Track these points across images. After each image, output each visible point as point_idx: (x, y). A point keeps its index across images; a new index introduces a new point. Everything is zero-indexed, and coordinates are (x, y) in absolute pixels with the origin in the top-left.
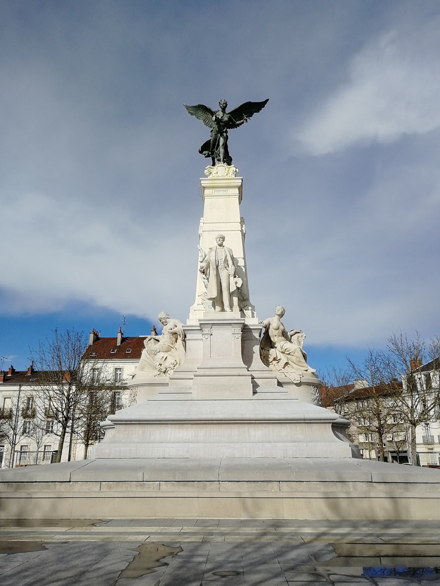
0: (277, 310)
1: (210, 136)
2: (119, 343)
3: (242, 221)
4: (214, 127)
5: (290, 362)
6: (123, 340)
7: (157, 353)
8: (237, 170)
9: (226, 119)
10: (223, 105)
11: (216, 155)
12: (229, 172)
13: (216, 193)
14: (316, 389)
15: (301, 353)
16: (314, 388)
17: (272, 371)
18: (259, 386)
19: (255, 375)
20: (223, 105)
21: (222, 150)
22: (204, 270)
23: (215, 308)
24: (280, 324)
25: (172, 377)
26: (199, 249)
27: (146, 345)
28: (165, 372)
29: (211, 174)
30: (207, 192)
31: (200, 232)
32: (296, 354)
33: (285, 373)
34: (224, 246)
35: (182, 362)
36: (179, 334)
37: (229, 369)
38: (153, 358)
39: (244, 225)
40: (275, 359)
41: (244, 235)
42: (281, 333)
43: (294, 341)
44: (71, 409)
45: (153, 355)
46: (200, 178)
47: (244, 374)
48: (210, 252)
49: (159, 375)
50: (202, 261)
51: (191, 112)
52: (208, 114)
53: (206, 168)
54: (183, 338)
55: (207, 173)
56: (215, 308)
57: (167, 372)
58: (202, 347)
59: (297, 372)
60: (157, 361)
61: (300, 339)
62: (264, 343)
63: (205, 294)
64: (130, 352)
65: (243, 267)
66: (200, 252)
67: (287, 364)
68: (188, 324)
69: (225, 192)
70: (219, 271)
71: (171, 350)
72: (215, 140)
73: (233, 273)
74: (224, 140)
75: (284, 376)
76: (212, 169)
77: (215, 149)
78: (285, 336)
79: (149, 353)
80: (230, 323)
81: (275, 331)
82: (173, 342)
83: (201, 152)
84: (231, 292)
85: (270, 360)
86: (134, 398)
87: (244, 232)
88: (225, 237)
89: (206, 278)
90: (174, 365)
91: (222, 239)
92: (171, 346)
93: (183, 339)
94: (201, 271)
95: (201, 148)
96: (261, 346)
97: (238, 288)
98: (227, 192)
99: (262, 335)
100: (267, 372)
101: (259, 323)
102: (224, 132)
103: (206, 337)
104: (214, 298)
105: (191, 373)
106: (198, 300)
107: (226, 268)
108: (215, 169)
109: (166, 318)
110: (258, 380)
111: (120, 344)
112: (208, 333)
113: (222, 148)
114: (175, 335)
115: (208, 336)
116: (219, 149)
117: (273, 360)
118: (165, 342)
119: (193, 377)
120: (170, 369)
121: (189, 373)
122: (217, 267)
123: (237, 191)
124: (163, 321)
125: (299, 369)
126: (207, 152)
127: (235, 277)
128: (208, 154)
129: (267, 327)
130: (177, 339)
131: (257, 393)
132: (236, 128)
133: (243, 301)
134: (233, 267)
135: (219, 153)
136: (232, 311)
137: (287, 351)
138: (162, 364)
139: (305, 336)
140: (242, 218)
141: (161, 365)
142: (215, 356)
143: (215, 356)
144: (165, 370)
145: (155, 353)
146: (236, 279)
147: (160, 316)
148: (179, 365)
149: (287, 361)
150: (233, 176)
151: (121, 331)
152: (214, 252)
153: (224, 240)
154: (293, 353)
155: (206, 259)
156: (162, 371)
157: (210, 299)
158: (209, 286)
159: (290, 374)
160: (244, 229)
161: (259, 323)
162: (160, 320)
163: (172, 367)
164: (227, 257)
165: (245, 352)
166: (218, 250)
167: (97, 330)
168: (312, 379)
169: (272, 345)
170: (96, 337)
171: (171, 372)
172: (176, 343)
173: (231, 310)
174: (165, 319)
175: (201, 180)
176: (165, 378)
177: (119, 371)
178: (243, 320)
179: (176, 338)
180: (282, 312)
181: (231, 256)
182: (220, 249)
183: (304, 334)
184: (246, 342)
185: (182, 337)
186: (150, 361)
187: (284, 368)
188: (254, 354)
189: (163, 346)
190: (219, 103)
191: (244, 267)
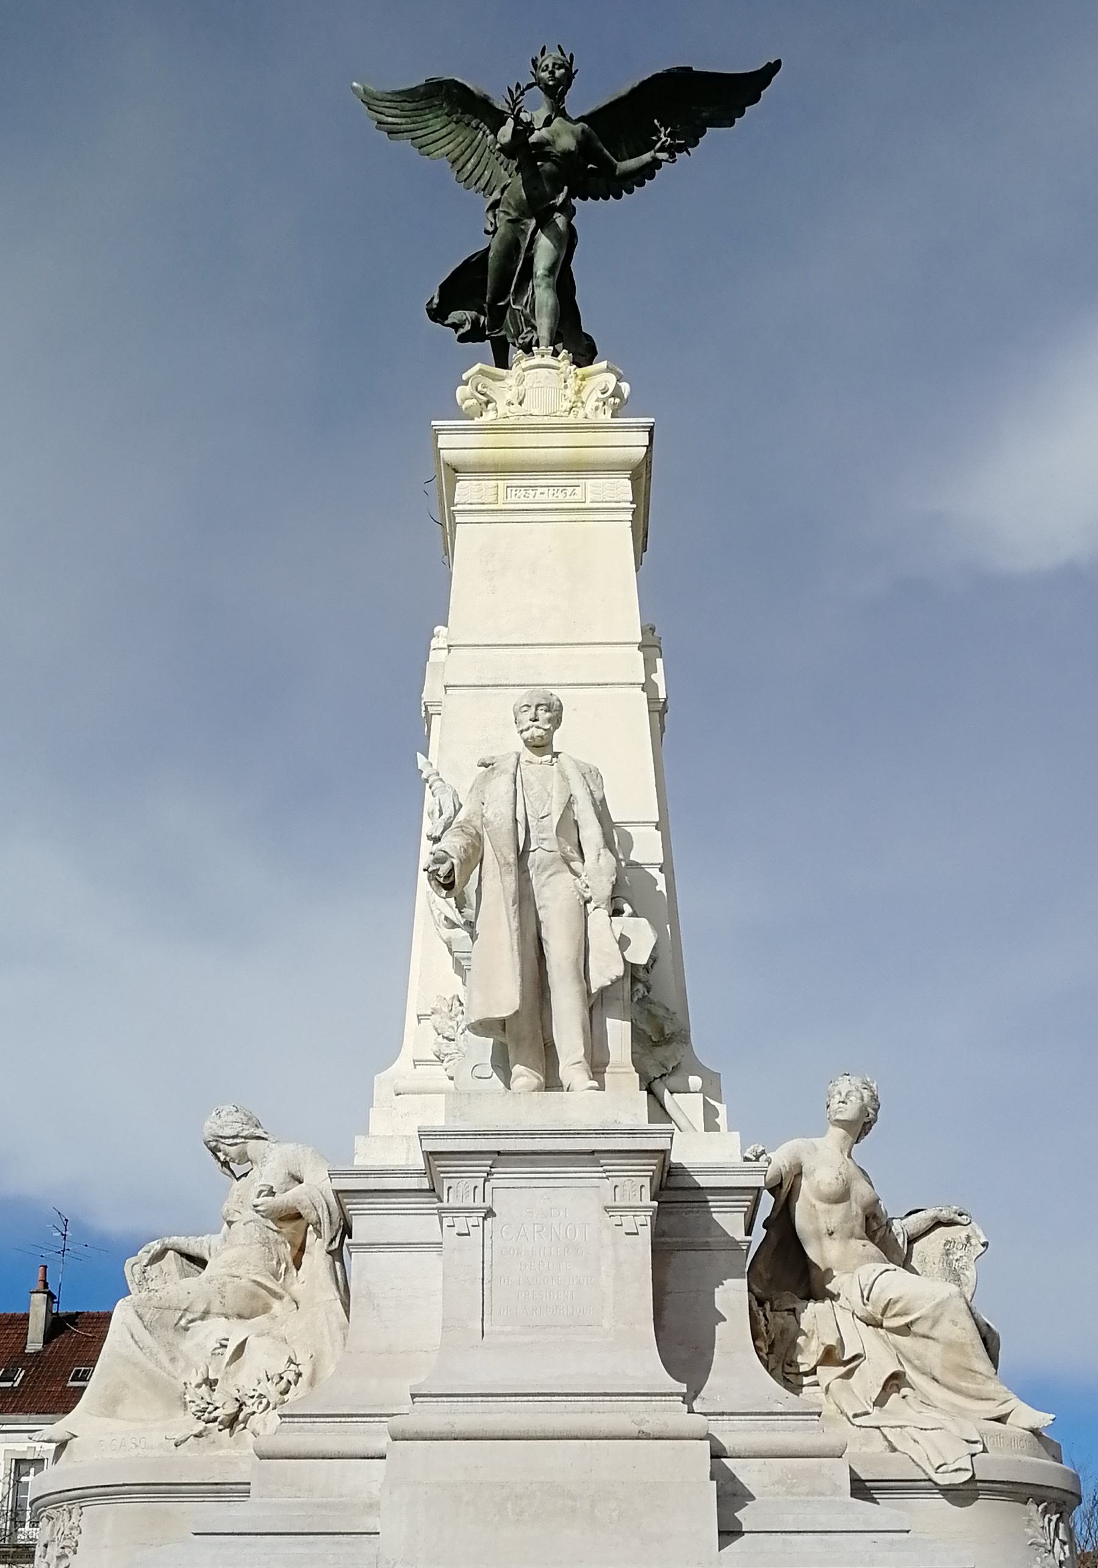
0: (838, 1098)
1: (487, 232)
2: (35, 1342)
3: (650, 644)
4: (505, 187)
5: (911, 1375)
7: (192, 1321)
8: (625, 387)
9: (566, 142)
10: (552, 73)
11: (515, 324)
13: (514, 499)
14: (1055, 1518)
15: (970, 1324)
16: (1045, 1512)
17: (819, 1414)
18: (752, 1498)
19: (730, 1435)
20: (552, 73)
21: (543, 296)
22: (452, 870)
23: (507, 1079)
24: (853, 1169)
25: (267, 1447)
26: (424, 776)
27: (139, 1284)
28: (232, 1422)
29: (490, 406)
30: (467, 490)
31: (431, 691)
32: (943, 1330)
33: (886, 1431)
34: (556, 755)
35: (329, 1370)
36: (313, 1217)
37: (584, 1403)
38: (170, 1347)
39: (660, 662)
40: (830, 1356)
41: (659, 711)
42: (861, 1220)
43: (928, 1269)
45: (170, 1335)
46: (433, 423)
47: (671, 1431)
48: (485, 779)
49: (198, 1436)
50: (438, 834)
51: (390, 119)
52: (477, 128)
53: (465, 377)
54: (333, 1240)
55: (468, 403)
56: (507, 1079)
57: (245, 1421)
58: (438, 1283)
59: (949, 1425)
60: (188, 1366)
61: (959, 1253)
62: (767, 1276)
63: (457, 1008)
65: (655, 872)
66: (428, 791)
67: (895, 1381)
68: (359, 1162)
69: (561, 496)
70: (529, 880)
71: (266, 1309)
72: (511, 248)
73: (607, 890)
74: (558, 247)
75: (880, 1445)
76: (498, 384)
77: (511, 298)
78: (877, 1241)
79: (146, 1318)
80: (593, 1152)
81: (826, 1206)
82: (279, 1263)
83: (438, 314)
84: (594, 991)
85: (806, 1360)
87: (662, 695)
88: (561, 706)
89: (463, 921)
90: (283, 1384)
91: (548, 715)
92: (269, 1284)
93: (336, 1245)
94: (433, 875)
95: (436, 294)
96: (754, 1287)
97: (632, 970)
98: (573, 494)
99: (759, 1233)
100: (791, 1422)
101: (746, 1159)
102: (554, 209)
103: (461, 1223)
104: (503, 1022)
105: (375, 1426)
107: (567, 861)
108: (511, 381)
109: (245, 1138)
110: (744, 1467)
111: (39, 1346)
113: (544, 285)
114: (288, 1228)
115: (473, 1221)
116: (530, 292)
117: (821, 1363)
118: (238, 1262)
119: (383, 1443)
120: (262, 1407)
121: (362, 1426)
122: (522, 855)
123: (622, 488)
124: (226, 1154)
125: (962, 1412)
126: (469, 315)
127: (617, 912)
128: (475, 322)
129: (786, 1188)
130: (302, 1249)
131: (741, 1533)
132: (618, 196)
133: (656, 1044)
134: (607, 861)
135: (533, 310)
136: (602, 1087)
137: (894, 1316)
138: (216, 1381)
139: (983, 1240)
140: (648, 630)
141: (211, 1384)
142: (509, 1328)
143: (509, 1328)
144: (231, 1408)
145: (183, 1322)
146: (624, 924)
147: (212, 1126)
148: (312, 1384)
149: (895, 1368)
150: (606, 417)
151: (46, 1285)
152: (507, 779)
153: (556, 721)
154: (929, 1323)
155: (461, 816)
156: (215, 1414)
157: (482, 1027)
158: (475, 967)
159: (917, 1435)
160: (659, 678)
161: (746, 1159)
162: (214, 1151)
163: (274, 1396)
164: (575, 808)
165: (666, 1313)
166: (526, 771)
168: (1032, 1464)
169: (809, 1282)
172: (298, 1269)
173: (595, 1084)
174: (238, 1141)
175: (436, 433)
176: (233, 1453)
177: (32, 1471)
178: (662, 1133)
179: (299, 1241)
180: (863, 1110)
181: (594, 804)
182: (535, 767)
183: (979, 1232)
184: (678, 1260)
185: (327, 1235)
186: (151, 1365)
187: (880, 1402)
188: (721, 1324)
189: (224, 1285)
190: (534, 62)
191: (661, 870)
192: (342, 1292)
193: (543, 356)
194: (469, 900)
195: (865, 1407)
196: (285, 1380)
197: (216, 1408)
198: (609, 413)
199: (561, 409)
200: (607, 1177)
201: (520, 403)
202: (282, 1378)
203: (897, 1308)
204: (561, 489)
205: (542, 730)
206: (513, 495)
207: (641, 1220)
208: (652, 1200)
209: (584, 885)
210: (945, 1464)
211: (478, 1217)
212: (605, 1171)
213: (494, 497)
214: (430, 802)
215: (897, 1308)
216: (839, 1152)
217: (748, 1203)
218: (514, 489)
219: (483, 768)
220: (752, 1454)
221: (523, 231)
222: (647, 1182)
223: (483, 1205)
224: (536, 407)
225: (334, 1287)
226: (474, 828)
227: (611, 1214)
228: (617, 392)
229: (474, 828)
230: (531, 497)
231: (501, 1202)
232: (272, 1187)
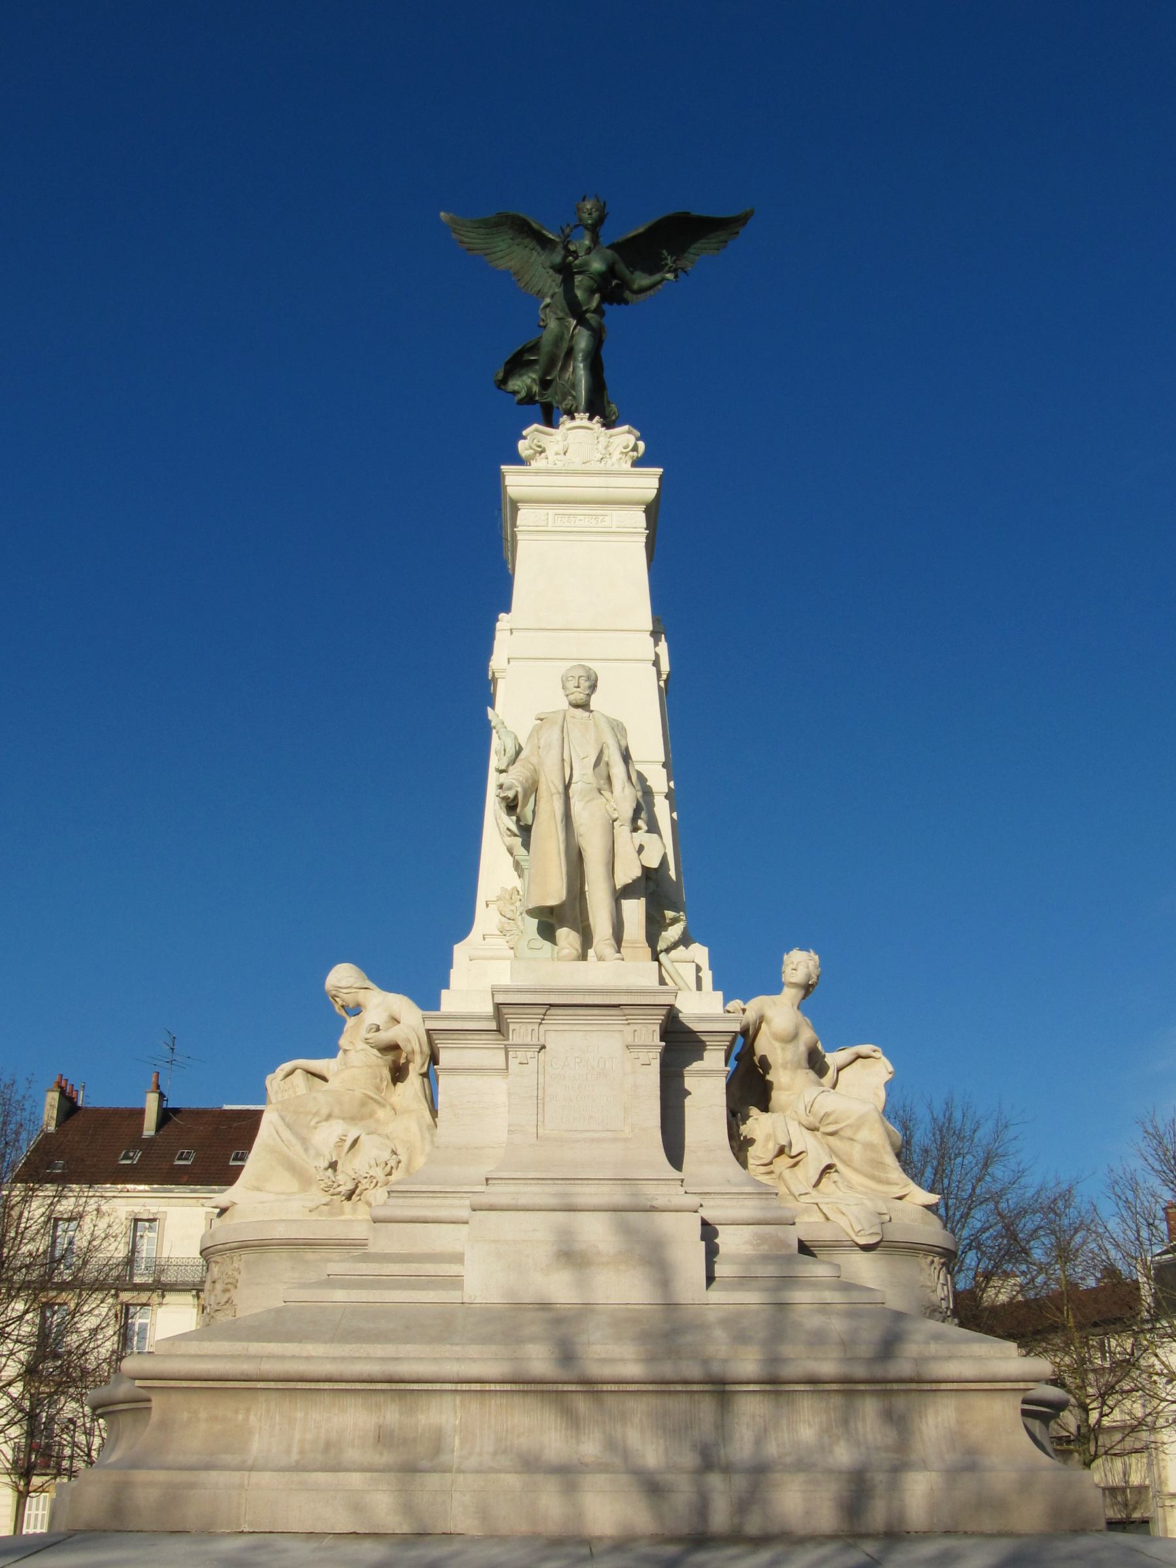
5: (839, 1166)
6: (166, 1116)
7: (318, 1123)
12: (611, 449)
21: (580, 372)
25: (381, 1213)
34: (592, 711)
44: (1104, 1283)
50: (503, 767)
54: (423, 1064)
57: (360, 1195)
64: (189, 1163)
79: (287, 1120)
84: (618, 887)
86: (227, 1295)
90: (388, 1168)
97: (646, 870)
106: (485, 918)
107: (599, 791)
111: (152, 1133)
112: (528, 1040)
115: (529, 1054)
119: (465, 1213)
127: (635, 829)
144: (350, 1186)
145: (313, 1123)
150: (627, 466)
153: (593, 687)
156: (339, 1189)
166: (569, 724)
167: (74, 1080)
170: (68, 1105)
171: (378, 1195)
181: (620, 750)
192: (429, 1103)
193: (582, 419)
194: (525, 817)
195: (807, 1189)
196: (389, 1166)
197: (339, 1186)
198: (629, 463)
199: (594, 459)
200: (629, 1024)
201: (565, 454)
202: (387, 1164)
203: (831, 1119)
204: (594, 517)
205: (582, 695)
206: (559, 521)
207: (651, 1055)
208: (661, 1041)
209: (613, 809)
210: (863, 1230)
211: (534, 1051)
212: (627, 1020)
213: (546, 522)
214: (495, 743)
215: (831, 1119)
216: (791, 1006)
217: (728, 1043)
218: (560, 516)
219: (539, 721)
220: (744, 1222)
221: (566, 327)
222: (657, 1028)
223: (538, 1043)
224: (575, 460)
225: (424, 1100)
226: (533, 765)
227: (631, 1050)
228: (635, 449)
229: (533, 765)
230: (572, 522)
231: (552, 1040)
232: (379, 1026)
